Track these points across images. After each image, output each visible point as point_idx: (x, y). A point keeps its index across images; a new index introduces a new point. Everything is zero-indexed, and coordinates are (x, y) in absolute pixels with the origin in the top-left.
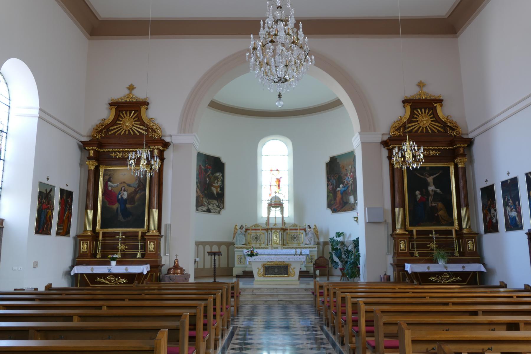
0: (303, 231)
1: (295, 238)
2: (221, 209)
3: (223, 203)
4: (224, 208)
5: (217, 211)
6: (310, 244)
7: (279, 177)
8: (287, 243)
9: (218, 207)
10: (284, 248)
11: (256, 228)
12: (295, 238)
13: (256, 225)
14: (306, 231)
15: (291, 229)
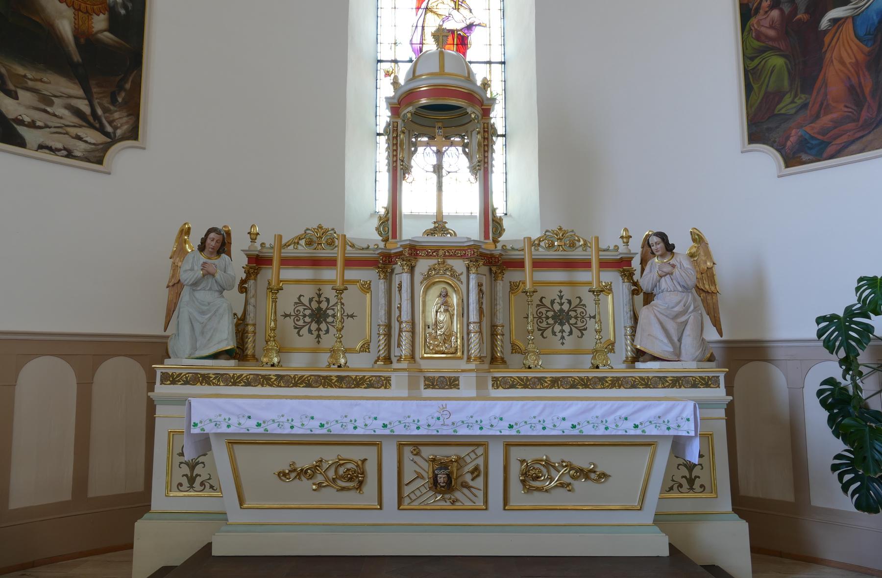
0: (611, 277)
1: (565, 317)
2: (113, 140)
3: (133, 107)
4: (133, 134)
5: (79, 148)
6: (677, 356)
7: (455, 24)
8: (515, 349)
9: (92, 121)
10: (498, 383)
11: (320, 249)
12: (561, 317)
13: (321, 237)
14: (628, 275)
15: (538, 264)
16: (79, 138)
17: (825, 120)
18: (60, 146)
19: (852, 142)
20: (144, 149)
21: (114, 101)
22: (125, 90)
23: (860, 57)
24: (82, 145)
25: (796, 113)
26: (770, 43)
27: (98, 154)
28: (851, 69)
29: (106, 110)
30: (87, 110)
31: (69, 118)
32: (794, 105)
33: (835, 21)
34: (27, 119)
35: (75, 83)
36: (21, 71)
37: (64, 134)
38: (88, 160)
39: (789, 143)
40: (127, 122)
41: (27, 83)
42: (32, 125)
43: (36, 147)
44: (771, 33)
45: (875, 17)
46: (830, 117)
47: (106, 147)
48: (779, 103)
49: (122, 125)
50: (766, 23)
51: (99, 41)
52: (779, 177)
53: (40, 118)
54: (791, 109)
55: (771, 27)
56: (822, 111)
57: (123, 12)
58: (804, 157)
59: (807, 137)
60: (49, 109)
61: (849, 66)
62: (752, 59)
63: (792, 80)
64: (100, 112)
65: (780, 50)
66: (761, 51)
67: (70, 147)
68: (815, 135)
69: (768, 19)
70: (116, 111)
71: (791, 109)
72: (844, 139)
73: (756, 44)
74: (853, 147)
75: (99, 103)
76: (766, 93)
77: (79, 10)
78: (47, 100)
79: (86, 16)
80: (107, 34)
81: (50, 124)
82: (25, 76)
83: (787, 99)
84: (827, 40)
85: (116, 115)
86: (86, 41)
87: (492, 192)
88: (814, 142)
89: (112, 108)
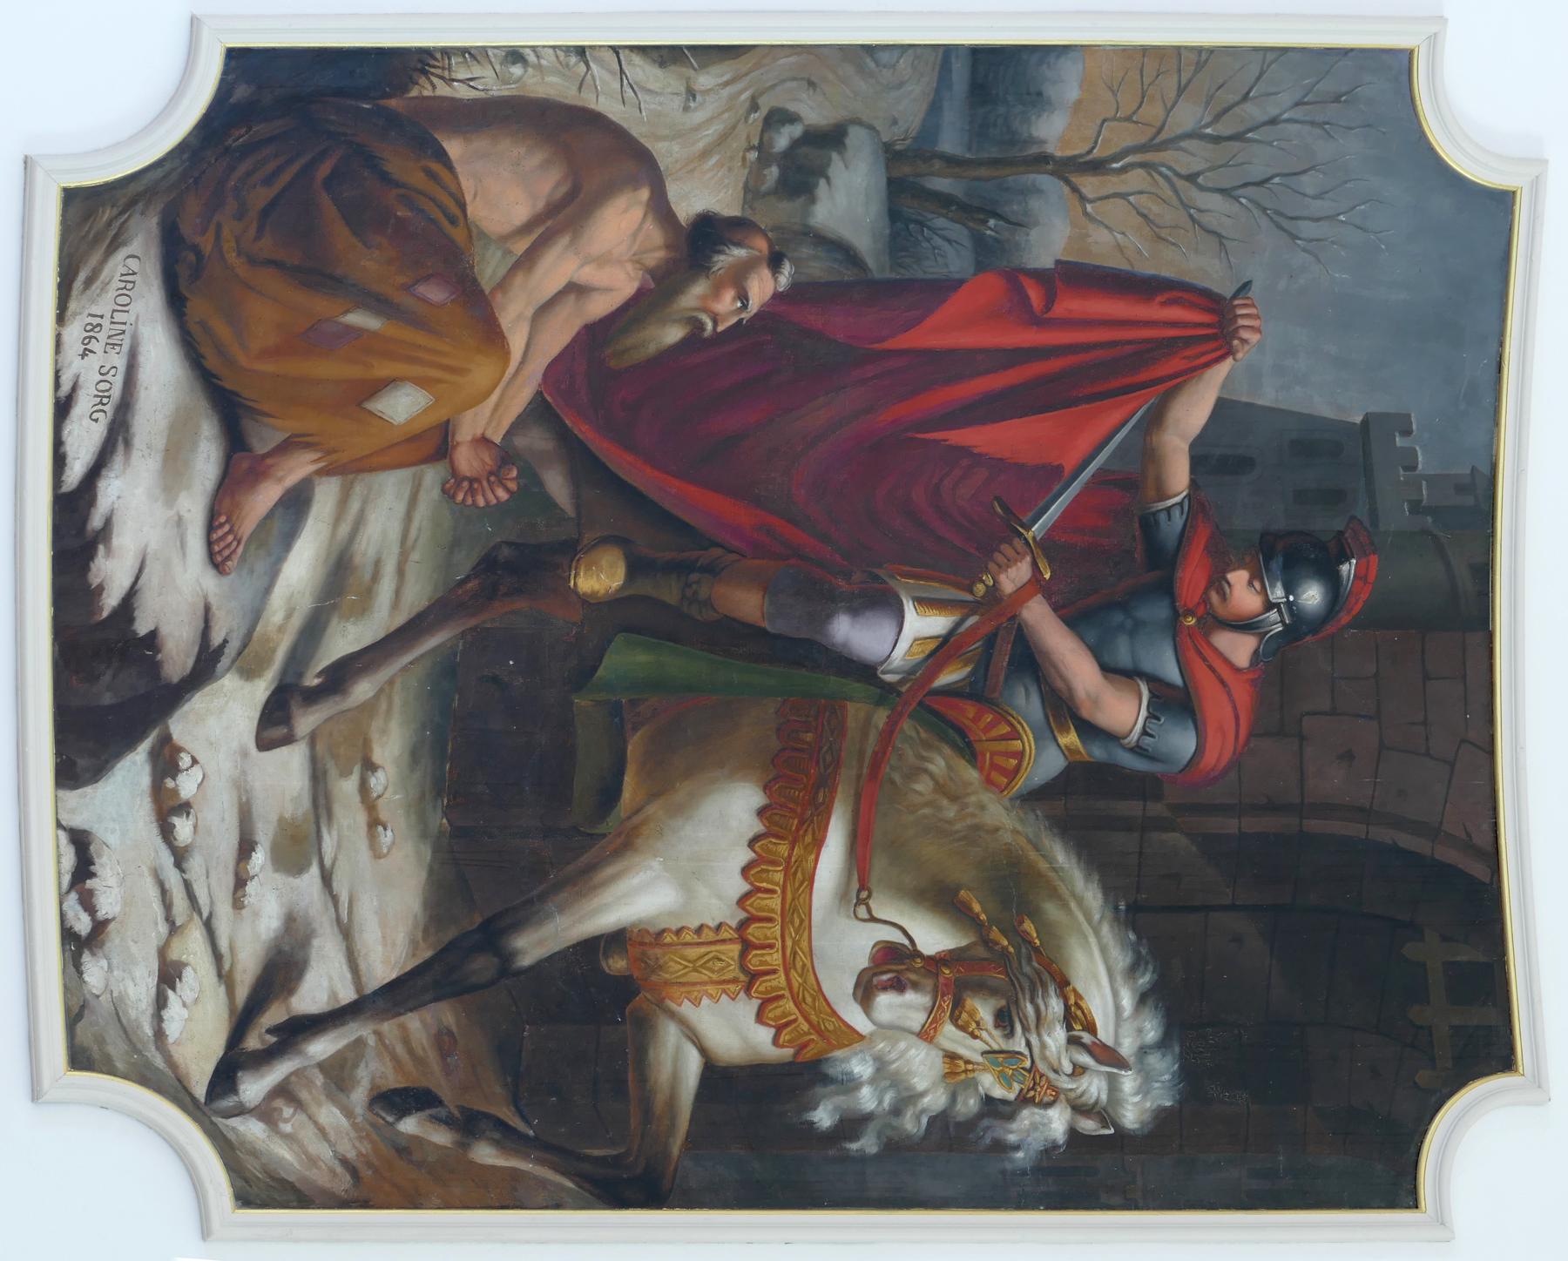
2: (213, 1101)
5: (124, 977)
9: (265, 1019)
16: (169, 975)
18: (108, 904)
21: (395, 1101)
22: (464, 1146)
24: (139, 988)
27: (116, 1049)
29: (338, 1073)
30: (323, 985)
31: (253, 934)
34: (186, 785)
35: (414, 944)
36: (391, 746)
37: (169, 919)
38: (75, 1016)
40: (313, 1161)
41: (345, 773)
42: (167, 808)
43: (78, 821)
47: (173, 1088)
49: (289, 1138)
51: (644, 1029)
53: (210, 828)
57: (823, 1117)
60: (259, 858)
64: (321, 1047)
67: (114, 939)
70: (348, 1113)
75: (359, 1043)
77: (747, 946)
78: (297, 848)
79: (734, 971)
80: (693, 1064)
81: (195, 864)
82: (369, 766)
85: (330, 1115)
86: (610, 992)
89: (359, 1097)
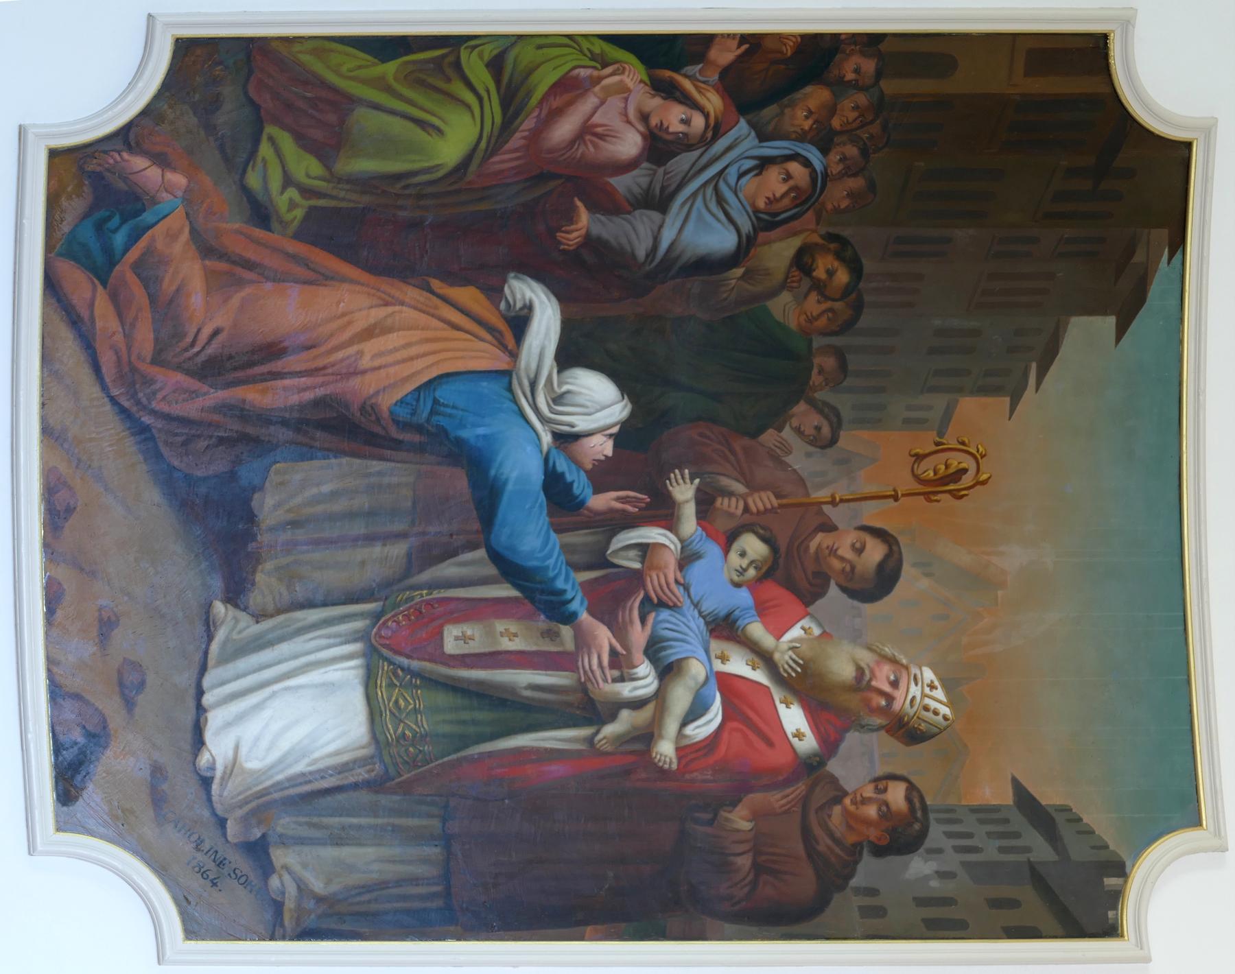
17: (188, 273)
19: (88, 345)
20: (31, 849)
23: (364, 386)
25: (245, 189)
26: (528, 124)
28: (340, 355)
32: (275, 182)
33: (520, 322)
39: (139, 163)
44: (564, 129)
45: (481, 431)
46: (197, 286)
48: (300, 139)
50: (608, 116)
52: (22, 132)
54: (265, 176)
55: (587, 130)
56: (223, 266)
58: (74, 207)
59: (147, 217)
61: (351, 350)
62: (496, 65)
63: (365, 183)
65: (493, 150)
66: (512, 98)
68: (142, 243)
69: (618, 124)
71: (265, 176)
72: (105, 318)
73: (545, 80)
74: (69, 346)
76: (354, 100)
83: (306, 167)
84: (467, 295)
87: (1216, 792)
88: (119, 239)
